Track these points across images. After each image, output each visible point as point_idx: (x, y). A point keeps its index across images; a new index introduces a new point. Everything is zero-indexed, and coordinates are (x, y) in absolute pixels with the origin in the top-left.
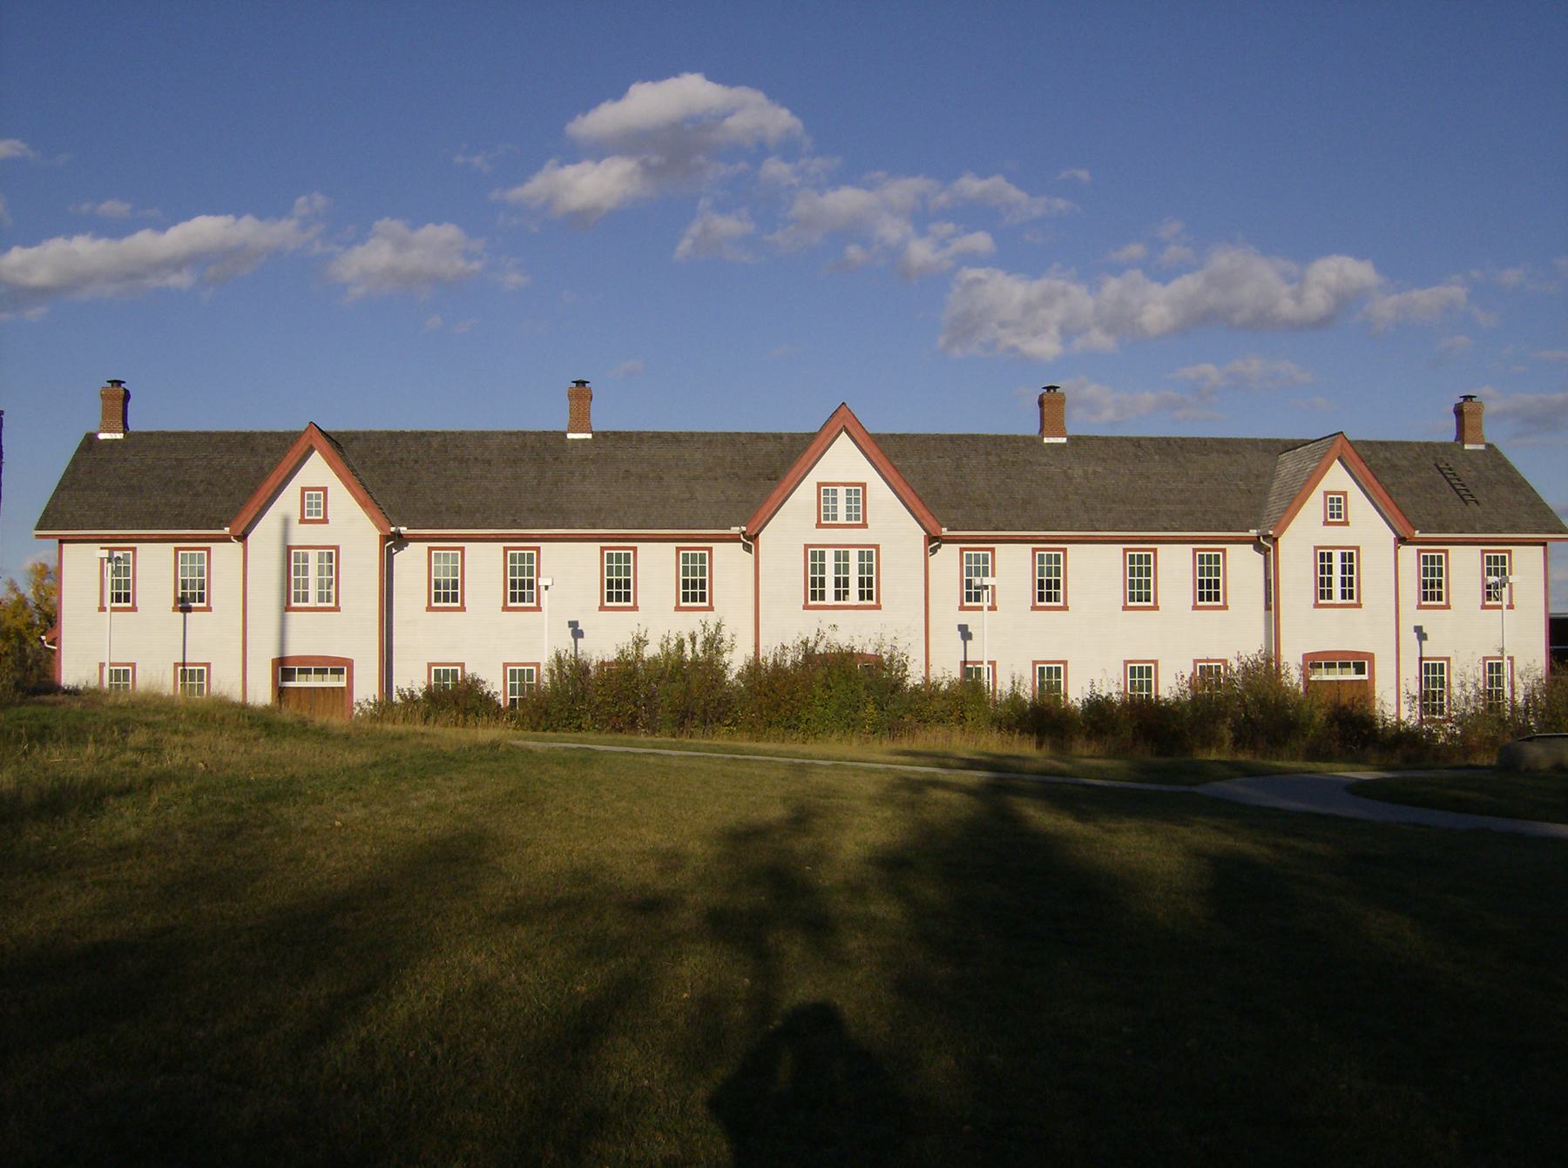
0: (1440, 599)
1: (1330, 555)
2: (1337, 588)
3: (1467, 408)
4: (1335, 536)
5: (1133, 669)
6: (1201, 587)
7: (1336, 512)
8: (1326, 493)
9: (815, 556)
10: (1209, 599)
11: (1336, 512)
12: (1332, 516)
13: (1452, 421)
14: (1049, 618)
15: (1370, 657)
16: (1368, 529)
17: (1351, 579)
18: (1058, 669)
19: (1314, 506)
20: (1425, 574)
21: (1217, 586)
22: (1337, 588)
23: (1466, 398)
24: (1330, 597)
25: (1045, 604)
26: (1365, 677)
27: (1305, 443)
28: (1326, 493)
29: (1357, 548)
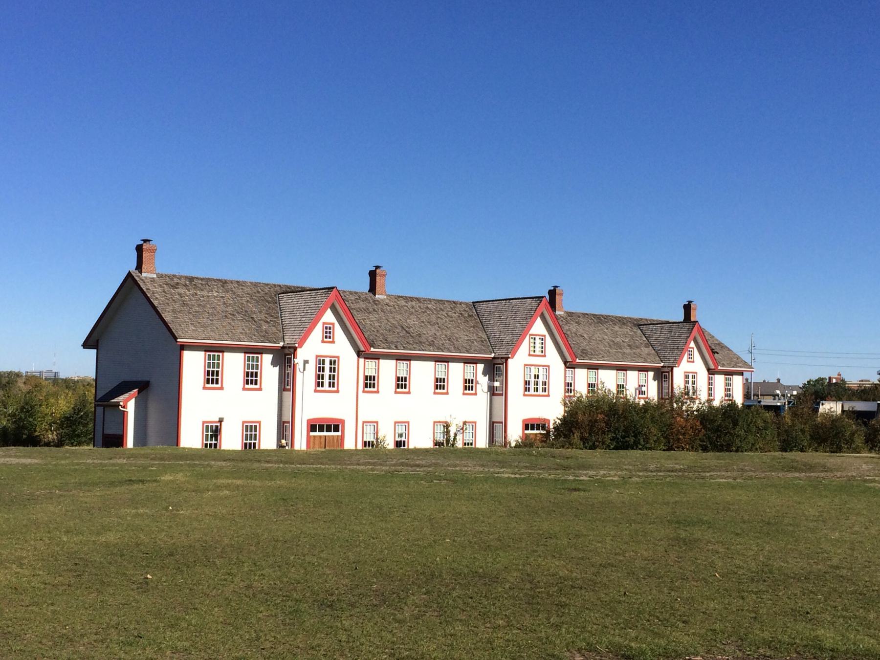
0: (374, 387)
1: (324, 361)
2: (326, 381)
3: (145, 246)
4: (328, 350)
5: (247, 426)
6: (208, 375)
7: (328, 336)
8: (324, 323)
9: (320, 361)
10: (212, 383)
11: (328, 336)
12: (326, 337)
13: (367, 279)
14: (213, 394)
15: (343, 422)
16: (342, 347)
17: (334, 376)
18: (256, 426)
19: (318, 332)
20: (209, 367)
21: (256, 376)
22: (326, 381)
23: (145, 241)
24: (322, 386)
25: (210, 385)
26: (339, 434)
27: (303, 290)
28: (324, 323)
29: (338, 357)
